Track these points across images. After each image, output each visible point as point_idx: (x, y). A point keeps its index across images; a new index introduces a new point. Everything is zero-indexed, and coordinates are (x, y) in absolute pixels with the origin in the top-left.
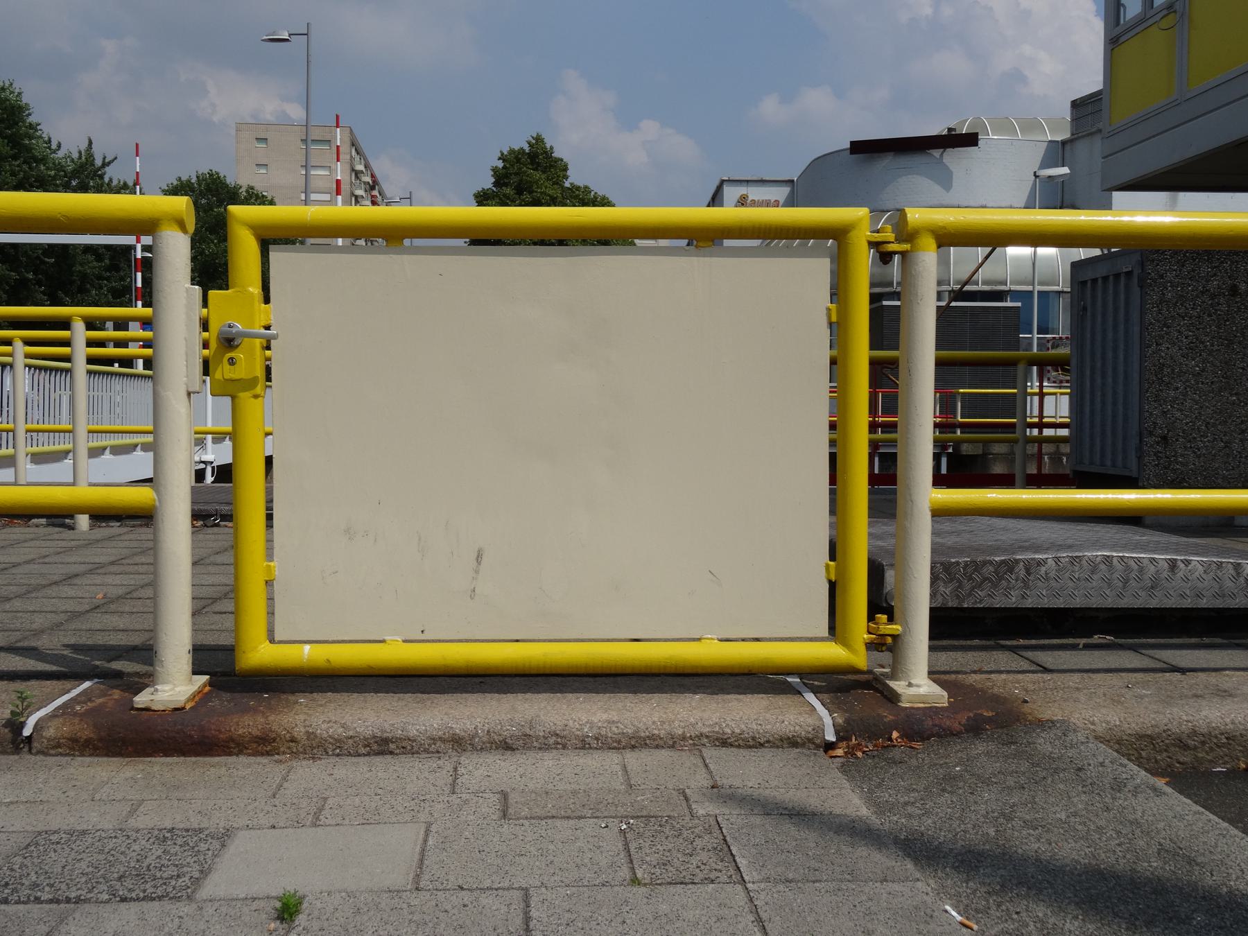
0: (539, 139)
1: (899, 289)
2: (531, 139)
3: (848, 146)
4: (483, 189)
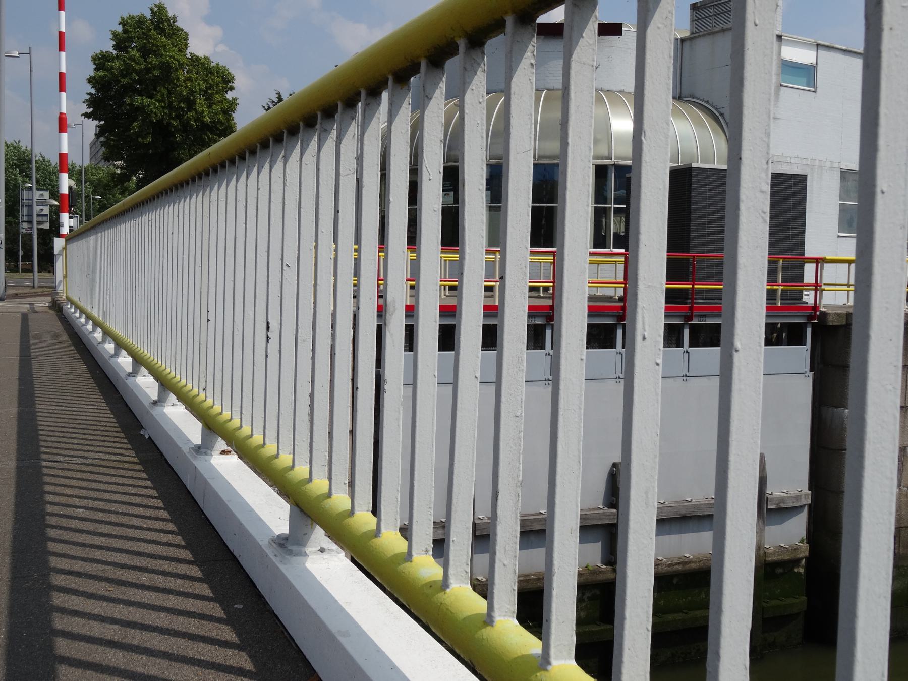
0: (161, 7)
2: (153, 6)
4: (102, 52)
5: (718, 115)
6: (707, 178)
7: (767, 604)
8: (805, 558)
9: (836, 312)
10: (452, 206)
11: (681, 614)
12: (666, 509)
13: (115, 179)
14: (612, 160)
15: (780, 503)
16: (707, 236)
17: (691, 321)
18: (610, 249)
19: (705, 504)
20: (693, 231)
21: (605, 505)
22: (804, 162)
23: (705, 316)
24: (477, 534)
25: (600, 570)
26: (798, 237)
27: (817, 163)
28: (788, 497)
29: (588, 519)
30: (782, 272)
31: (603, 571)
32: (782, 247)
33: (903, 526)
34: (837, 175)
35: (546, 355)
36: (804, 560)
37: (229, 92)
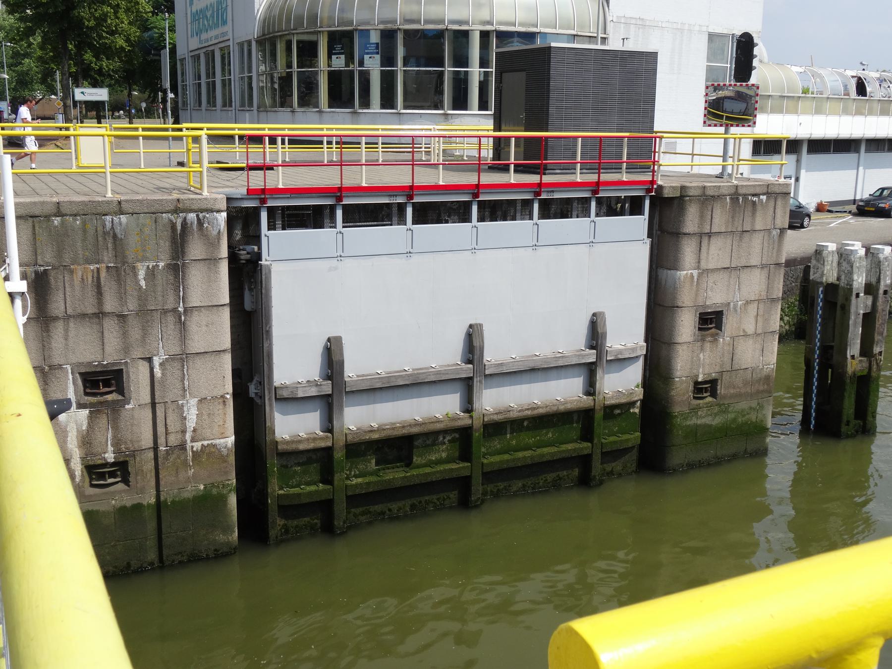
6: (565, 56)
7: (605, 440)
8: (640, 400)
9: (672, 185)
10: (343, 69)
11: (530, 452)
12: (517, 363)
13: (20, 33)
15: (618, 354)
16: (565, 111)
17: (540, 196)
19: (551, 357)
20: (551, 106)
21: (463, 361)
22: (675, 26)
23: (553, 191)
24: (347, 391)
25: (459, 417)
26: (649, 111)
27: (686, 27)
28: (625, 349)
29: (447, 374)
30: (627, 148)
31: (461, 418)
32: (634, 121)
33: (725, 370)
34: (705, 39)
35: (407, 230)
36: (639, 401)
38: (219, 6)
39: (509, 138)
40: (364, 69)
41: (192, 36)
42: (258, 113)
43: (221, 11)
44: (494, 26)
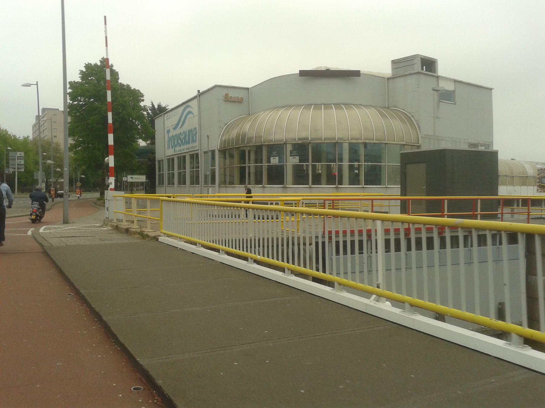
1: (421, 145)
3: (298, 72)
5: (410, 116)
10: (278, 164)
14: (362, 140)
18: (362, 185)
37: (142, 102)
38: (190, 133)
39: (477, 199)
40: (271, 164)
41: (169, 148)
42: (219, 188)
43: (192, 135)
44: (363, 140)
